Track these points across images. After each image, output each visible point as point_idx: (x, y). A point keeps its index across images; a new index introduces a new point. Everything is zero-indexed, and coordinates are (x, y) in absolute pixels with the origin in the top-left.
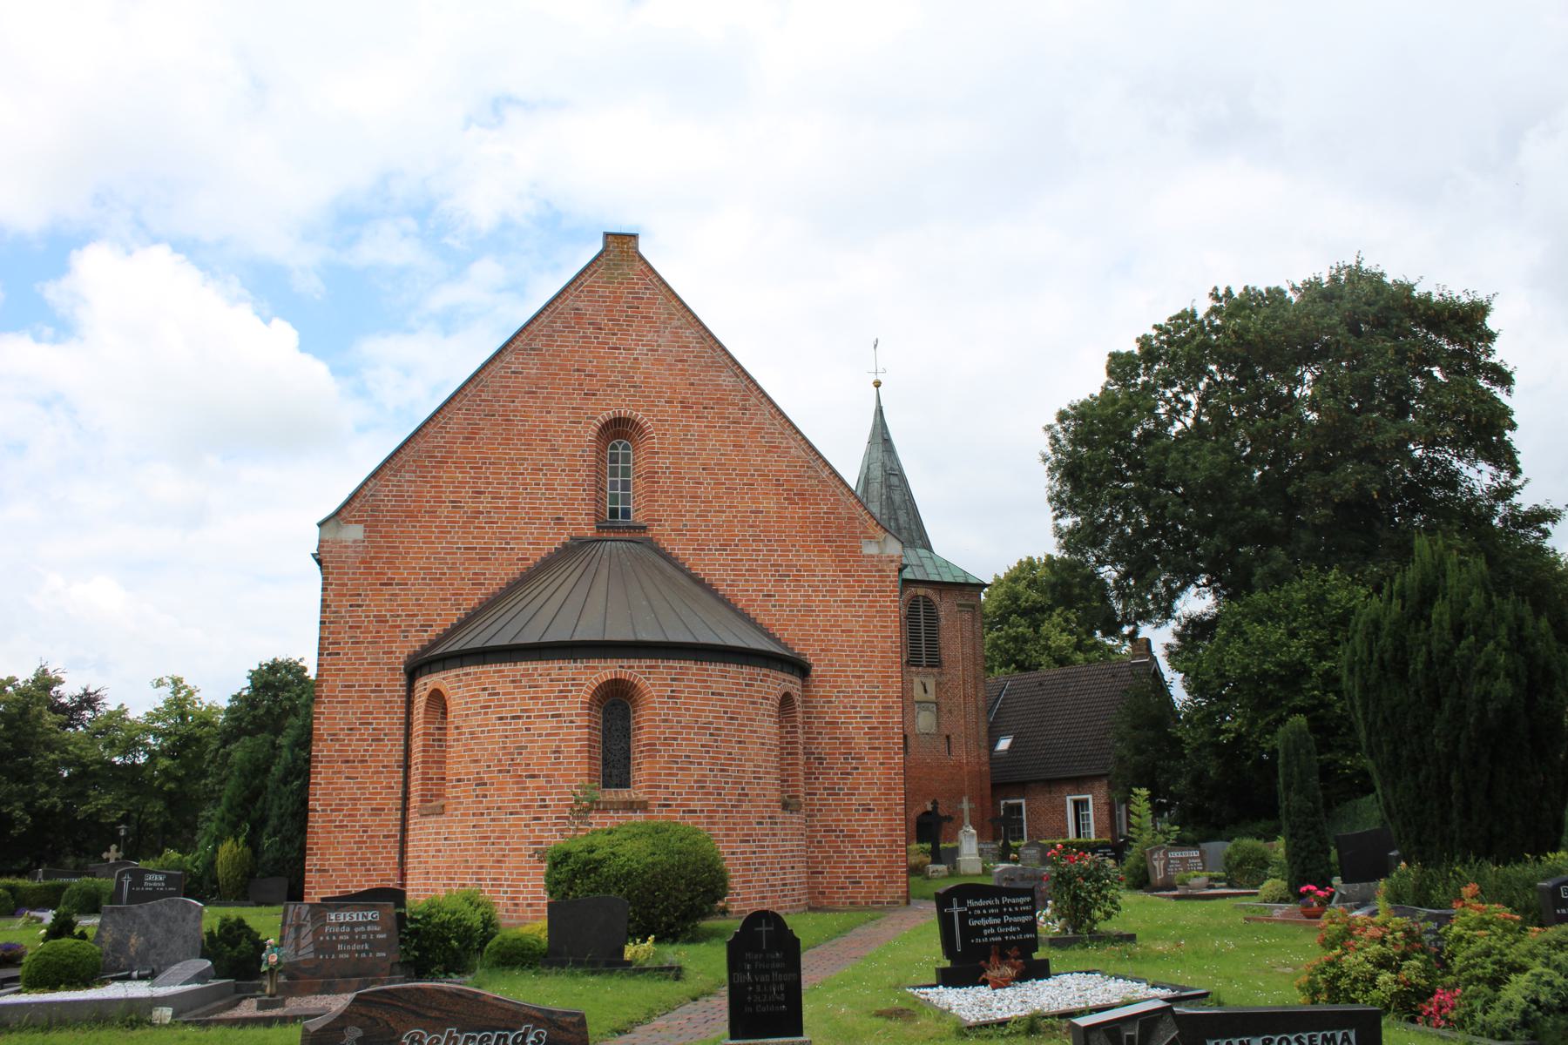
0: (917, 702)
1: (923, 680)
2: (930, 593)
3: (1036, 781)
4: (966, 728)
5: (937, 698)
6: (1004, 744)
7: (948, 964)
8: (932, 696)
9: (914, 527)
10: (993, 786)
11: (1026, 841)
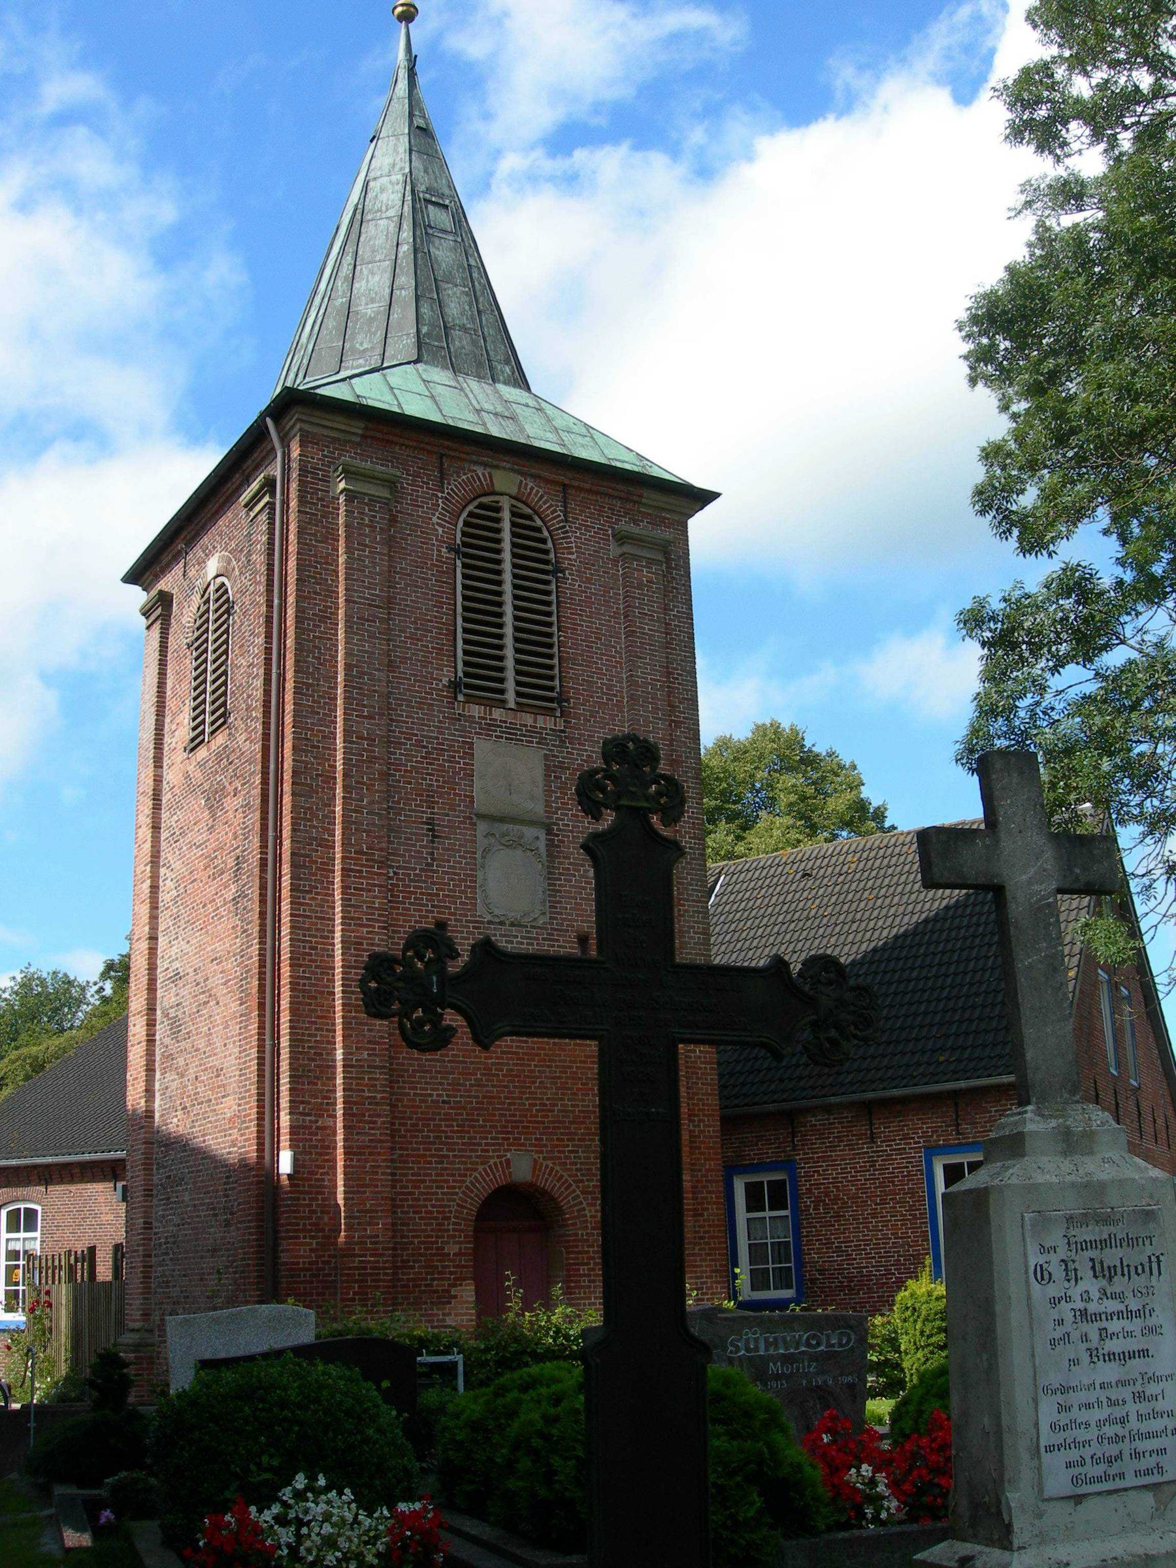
0: (482, 816)
5: (549, 811)
7: (795, 968)
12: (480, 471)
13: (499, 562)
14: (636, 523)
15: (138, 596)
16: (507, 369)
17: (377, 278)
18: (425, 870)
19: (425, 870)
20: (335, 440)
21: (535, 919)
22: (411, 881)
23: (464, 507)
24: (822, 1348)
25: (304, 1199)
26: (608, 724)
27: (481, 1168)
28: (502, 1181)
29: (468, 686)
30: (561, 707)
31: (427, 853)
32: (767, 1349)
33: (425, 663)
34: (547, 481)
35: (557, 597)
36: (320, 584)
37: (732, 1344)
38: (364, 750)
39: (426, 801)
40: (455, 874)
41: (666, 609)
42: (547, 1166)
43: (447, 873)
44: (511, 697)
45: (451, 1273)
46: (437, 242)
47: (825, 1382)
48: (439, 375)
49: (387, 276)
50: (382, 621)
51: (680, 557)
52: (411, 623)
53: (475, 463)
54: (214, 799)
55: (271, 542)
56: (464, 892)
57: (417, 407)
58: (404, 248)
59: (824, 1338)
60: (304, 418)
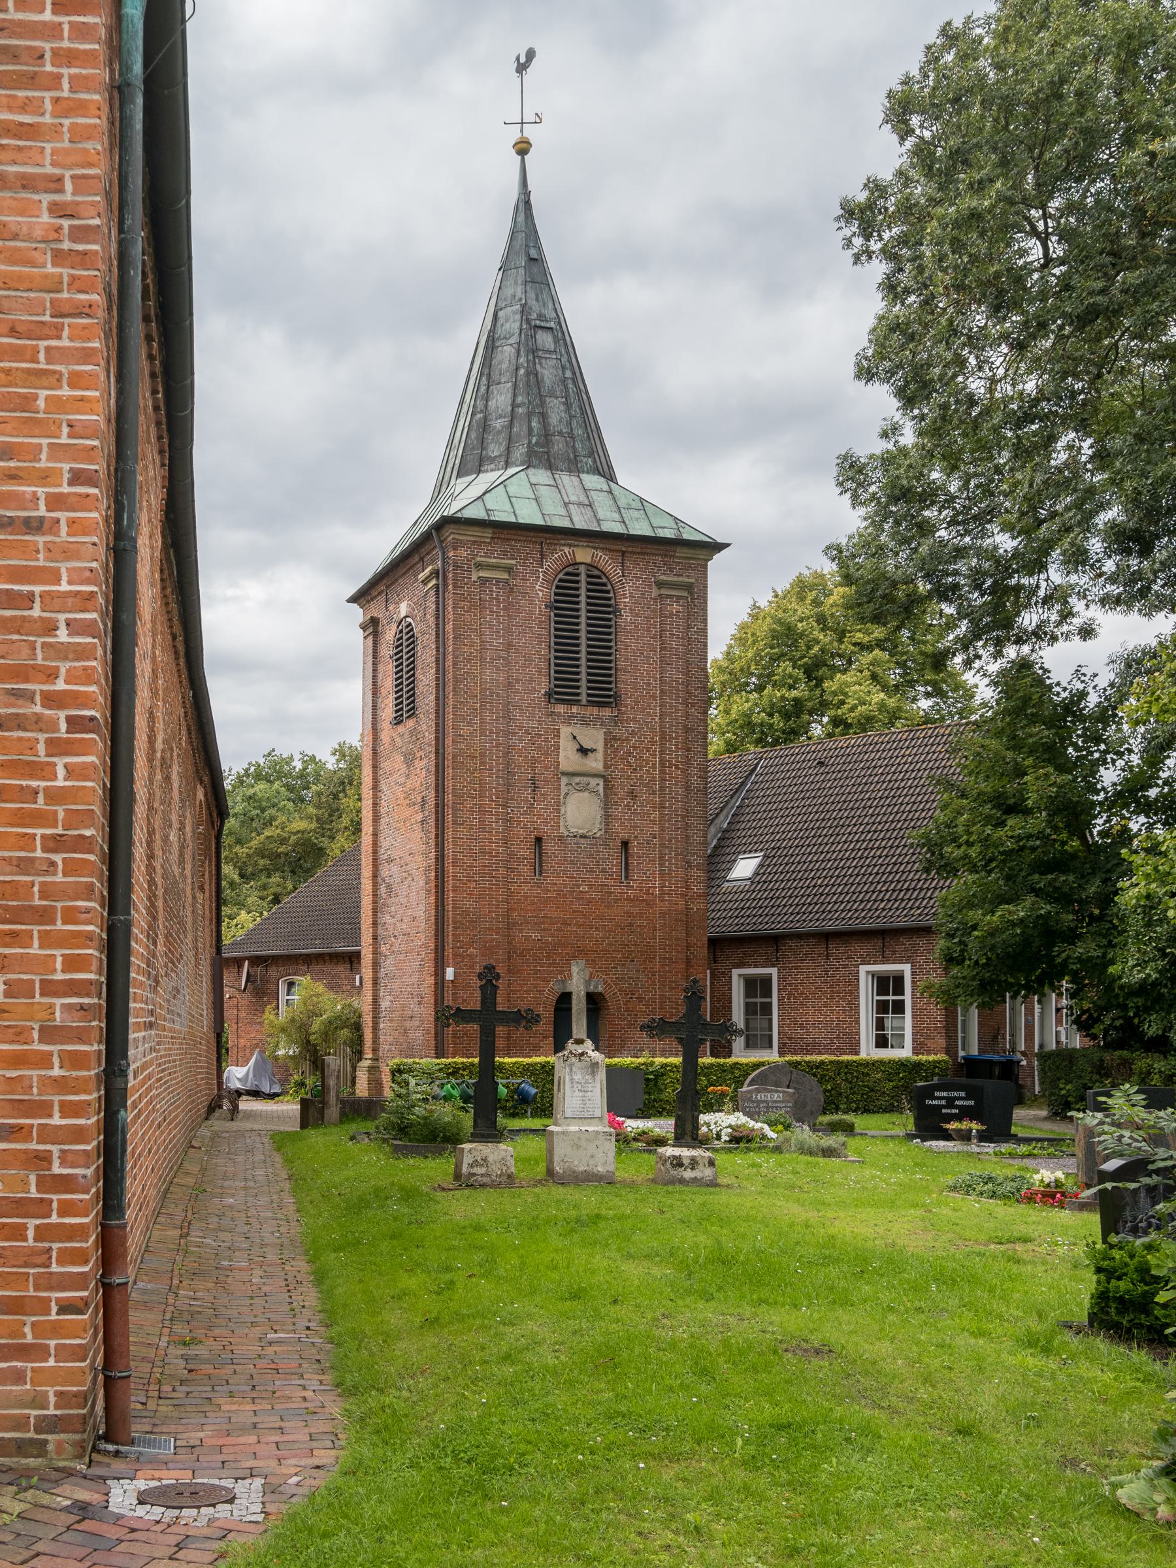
0: (563, 774)
3: (799, 936)
4: (662, 828)
5: (606, 767)
6: (745, 868)
12: (566, 550)
13: (578, 603)
15: (357, 614)
17: (503, 397)
29: (557, 693)
33: (531, 681)
34: (610, 550)
41: (688, 627)
54: (409, 760)
55: (437, 610)
58: (522, 371)
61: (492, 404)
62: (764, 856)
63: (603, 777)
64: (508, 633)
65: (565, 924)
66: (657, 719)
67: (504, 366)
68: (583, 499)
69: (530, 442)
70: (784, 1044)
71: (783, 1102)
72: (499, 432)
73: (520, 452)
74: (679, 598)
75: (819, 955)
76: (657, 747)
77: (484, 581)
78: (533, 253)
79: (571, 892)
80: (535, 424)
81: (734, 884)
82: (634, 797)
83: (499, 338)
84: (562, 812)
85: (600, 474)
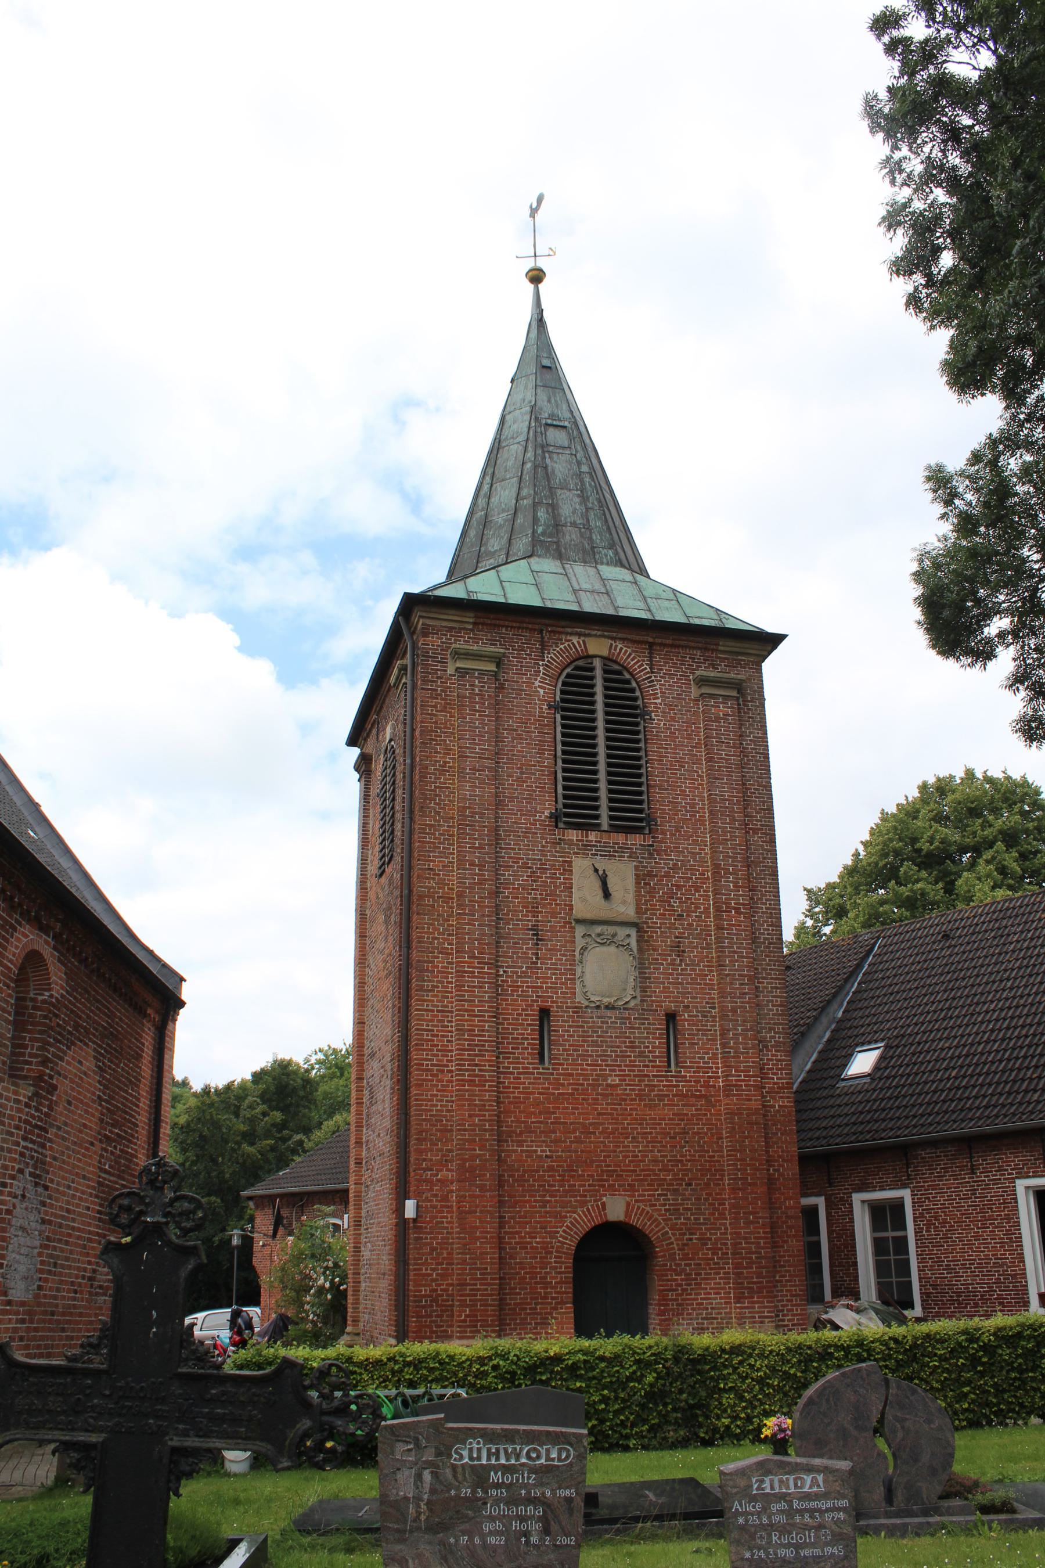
0: (578, 921)
1: (602, 864)
2: (625, 653)
3: (934, 1143)
4: (722, 994)
5: (639, 911)
6: (863, 1063)
8: (624, 904)
9: (596, 523)
10: (804, 1160)
11: (918, 1311)
14: (714, 667)
16: (610, 552)
17: (507, 492)
18: (531, 968)
19: (531, 968)
20: (451, 629)
21: (627, 1003)
22: (518, 977)
23: (562, 671)
24: (543, 1461)
25: (426, 1238)
26: (692, 836)
27: (579, 1211)
28: (598, 1221)
29: (567, 815)
30: (649, 825)
31: (533, 954)
32: (489, 1459)
33: (529, 800)
35: (645, 736)
36: (440, 745)
37: (456, 1452)
38: (476, 874)
39: (531, 912)
40: (556, 969)
42: (638, 1208)
43: (549, 969)
44: (605, 822)
45: (553, 1298)
46: (555, 456)
47: (543, 1494)
48: (547, 565)
49: (514, 490)
50: (490, 769)
51: (755, 691)
52: (518, 768)
53: (571, 634)
56: (565, 984)
57: (522, 595)
58: (529, 465)
59: (543, 1452)
60: (424, 614)
61: (494, 500)
62: (886, 1047)
63: (635, 925)
64: (498, 738)
65: (587, 1133)
66: (707, 850)
67: (510, 463)
68: (598, 586)
69: (534, 532)
70: (928, 1295)
71: (825, 1496)
72: (501, 526)
73: (522, 544)
74: (726, 698)
75: (962, 1169)
76: (710, 885)
77: (462, 672)
78: (546, 362)
79: (595, 1086)
80: (542, 514)
81: (851, 1083)
82: (680, 953)
83: (506, 439)
84: (578, 973)
85: (622, 566)
